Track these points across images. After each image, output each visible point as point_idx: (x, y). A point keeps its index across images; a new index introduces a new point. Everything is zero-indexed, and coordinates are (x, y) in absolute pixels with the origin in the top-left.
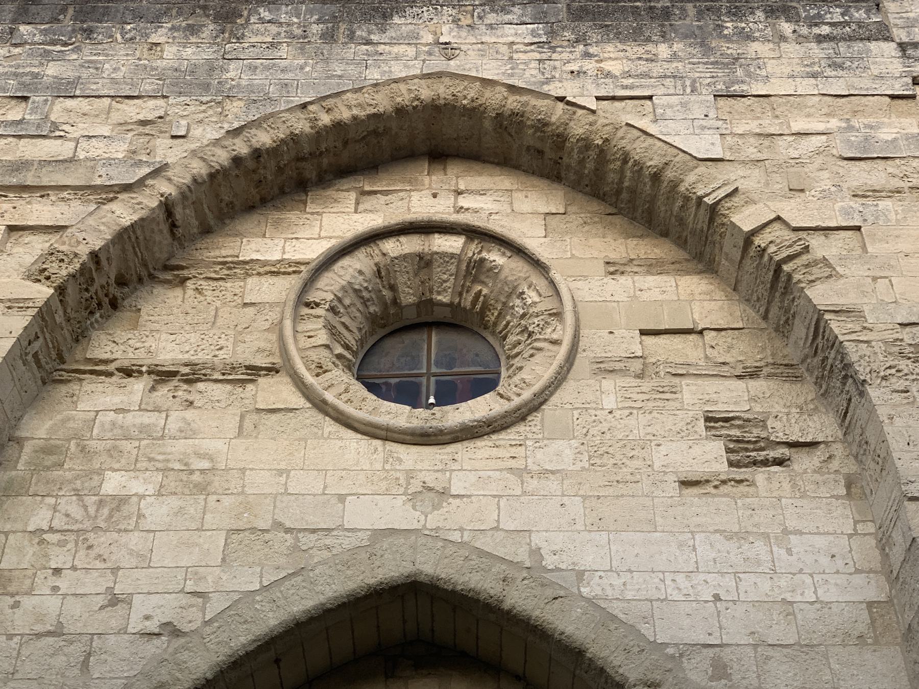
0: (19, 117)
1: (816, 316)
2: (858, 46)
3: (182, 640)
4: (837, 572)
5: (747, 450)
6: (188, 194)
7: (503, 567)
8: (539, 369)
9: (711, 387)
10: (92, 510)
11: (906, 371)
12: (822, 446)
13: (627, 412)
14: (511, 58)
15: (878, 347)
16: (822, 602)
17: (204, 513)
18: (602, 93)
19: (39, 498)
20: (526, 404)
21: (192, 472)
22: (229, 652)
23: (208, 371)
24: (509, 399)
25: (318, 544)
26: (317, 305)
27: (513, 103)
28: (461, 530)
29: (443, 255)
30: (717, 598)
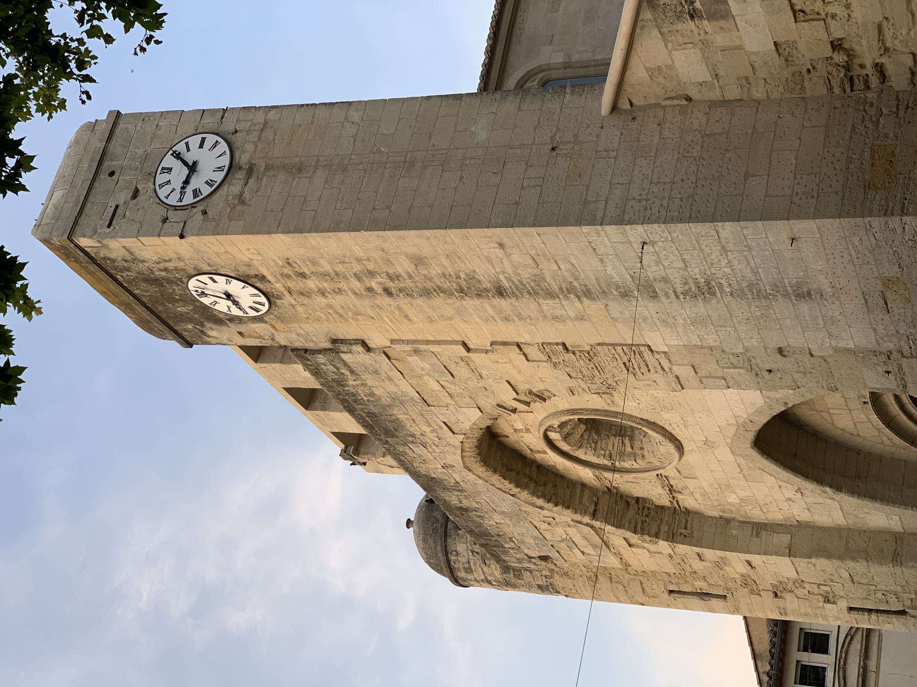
6: (583, 511)
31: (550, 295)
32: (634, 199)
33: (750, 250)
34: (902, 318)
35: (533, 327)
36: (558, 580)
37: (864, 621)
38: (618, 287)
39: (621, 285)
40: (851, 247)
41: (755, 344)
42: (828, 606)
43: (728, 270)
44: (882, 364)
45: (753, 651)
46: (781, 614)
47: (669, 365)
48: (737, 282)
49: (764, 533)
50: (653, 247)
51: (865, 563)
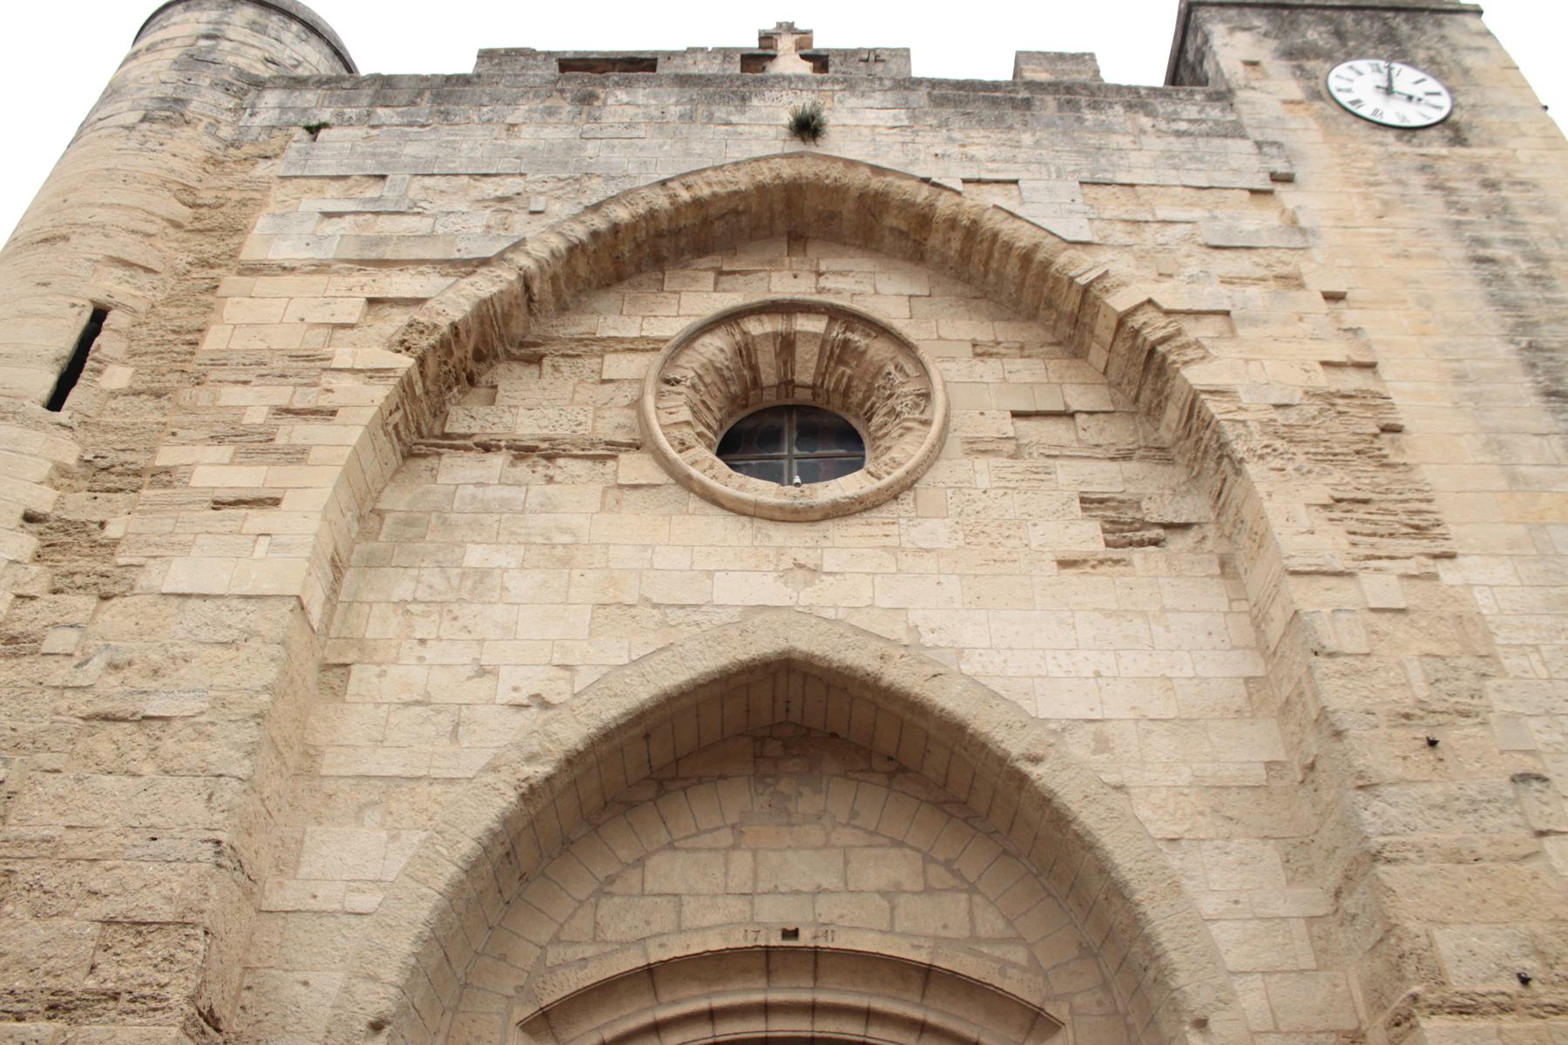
0: (376, 195)
1: (1191, 397)
2: (1216, 142)
3: (550, 713)
4: (1214, 649)
5: (1122, 531)
7: (881, 644)
8: (909, 449)
9: (1085, 467)
10: (455, 582)
11: (1281, 450)
12: (1196, 527)
13: (1001, 492)
14: (874, 140)
15: (1254, 427)
16: (1200, 677)
17: (568, 586)
18: (968, 176)
19: (401, 570)
20: (898, 481)
21: (554, 546)
22: (600, 724)
23: (568, 447)
24: (879, 478)
25: (686, 620)
26: (678, 382)
27: (876, 183)
28: (836, 607)
29: (805, 334)
30: (1098, 675)
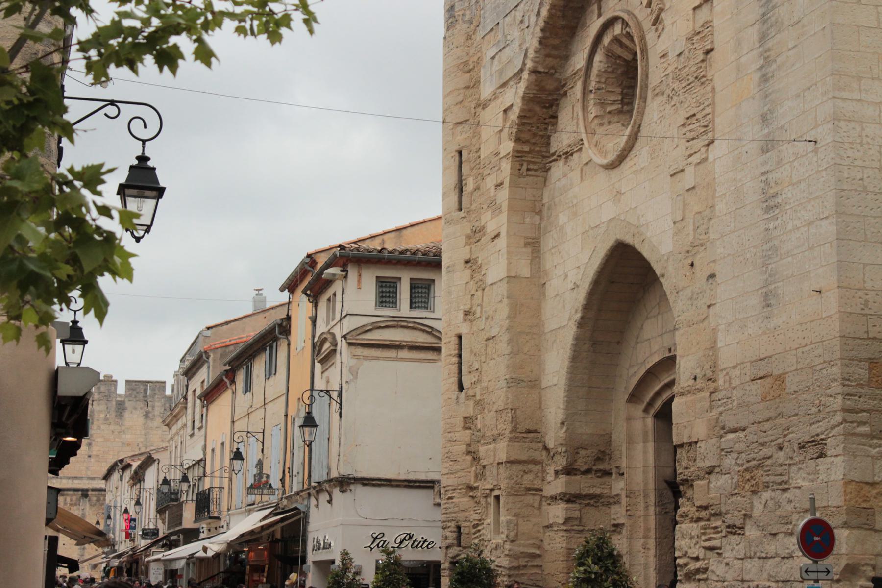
31: (763, 38)
32: (863, 129)
33: (811, 249)
34: (747, 392)
35: (729, 16)
36: (462, 27)
37: (448, 348)
38: (771, 111)
39: (775, 115)
40: (813, 346)
41: (719, 251)
42: (461, 315)
43: (790, 227)
44: (703, 373)
45: (405, 228)
46: (448, 267)
47: (694, 163)
48: (779, 236)
49: (529, 250)
50: (812, 151)
51: (507, 352)
